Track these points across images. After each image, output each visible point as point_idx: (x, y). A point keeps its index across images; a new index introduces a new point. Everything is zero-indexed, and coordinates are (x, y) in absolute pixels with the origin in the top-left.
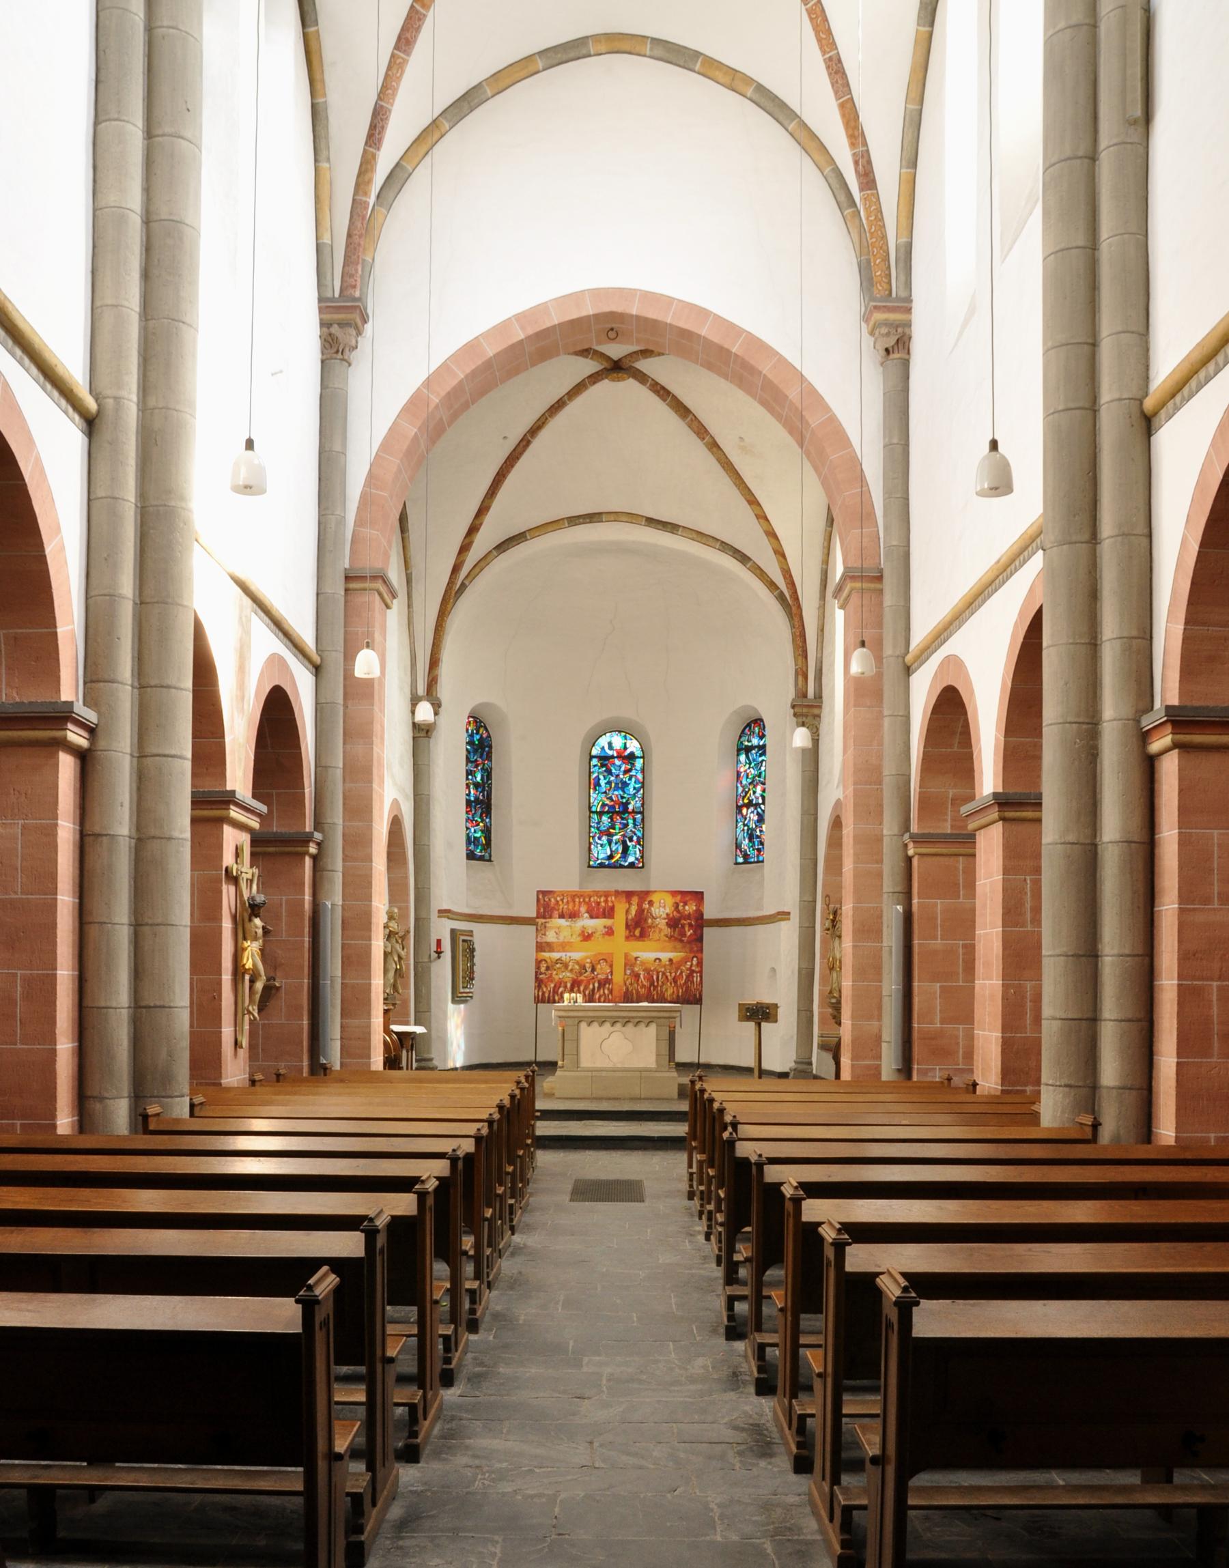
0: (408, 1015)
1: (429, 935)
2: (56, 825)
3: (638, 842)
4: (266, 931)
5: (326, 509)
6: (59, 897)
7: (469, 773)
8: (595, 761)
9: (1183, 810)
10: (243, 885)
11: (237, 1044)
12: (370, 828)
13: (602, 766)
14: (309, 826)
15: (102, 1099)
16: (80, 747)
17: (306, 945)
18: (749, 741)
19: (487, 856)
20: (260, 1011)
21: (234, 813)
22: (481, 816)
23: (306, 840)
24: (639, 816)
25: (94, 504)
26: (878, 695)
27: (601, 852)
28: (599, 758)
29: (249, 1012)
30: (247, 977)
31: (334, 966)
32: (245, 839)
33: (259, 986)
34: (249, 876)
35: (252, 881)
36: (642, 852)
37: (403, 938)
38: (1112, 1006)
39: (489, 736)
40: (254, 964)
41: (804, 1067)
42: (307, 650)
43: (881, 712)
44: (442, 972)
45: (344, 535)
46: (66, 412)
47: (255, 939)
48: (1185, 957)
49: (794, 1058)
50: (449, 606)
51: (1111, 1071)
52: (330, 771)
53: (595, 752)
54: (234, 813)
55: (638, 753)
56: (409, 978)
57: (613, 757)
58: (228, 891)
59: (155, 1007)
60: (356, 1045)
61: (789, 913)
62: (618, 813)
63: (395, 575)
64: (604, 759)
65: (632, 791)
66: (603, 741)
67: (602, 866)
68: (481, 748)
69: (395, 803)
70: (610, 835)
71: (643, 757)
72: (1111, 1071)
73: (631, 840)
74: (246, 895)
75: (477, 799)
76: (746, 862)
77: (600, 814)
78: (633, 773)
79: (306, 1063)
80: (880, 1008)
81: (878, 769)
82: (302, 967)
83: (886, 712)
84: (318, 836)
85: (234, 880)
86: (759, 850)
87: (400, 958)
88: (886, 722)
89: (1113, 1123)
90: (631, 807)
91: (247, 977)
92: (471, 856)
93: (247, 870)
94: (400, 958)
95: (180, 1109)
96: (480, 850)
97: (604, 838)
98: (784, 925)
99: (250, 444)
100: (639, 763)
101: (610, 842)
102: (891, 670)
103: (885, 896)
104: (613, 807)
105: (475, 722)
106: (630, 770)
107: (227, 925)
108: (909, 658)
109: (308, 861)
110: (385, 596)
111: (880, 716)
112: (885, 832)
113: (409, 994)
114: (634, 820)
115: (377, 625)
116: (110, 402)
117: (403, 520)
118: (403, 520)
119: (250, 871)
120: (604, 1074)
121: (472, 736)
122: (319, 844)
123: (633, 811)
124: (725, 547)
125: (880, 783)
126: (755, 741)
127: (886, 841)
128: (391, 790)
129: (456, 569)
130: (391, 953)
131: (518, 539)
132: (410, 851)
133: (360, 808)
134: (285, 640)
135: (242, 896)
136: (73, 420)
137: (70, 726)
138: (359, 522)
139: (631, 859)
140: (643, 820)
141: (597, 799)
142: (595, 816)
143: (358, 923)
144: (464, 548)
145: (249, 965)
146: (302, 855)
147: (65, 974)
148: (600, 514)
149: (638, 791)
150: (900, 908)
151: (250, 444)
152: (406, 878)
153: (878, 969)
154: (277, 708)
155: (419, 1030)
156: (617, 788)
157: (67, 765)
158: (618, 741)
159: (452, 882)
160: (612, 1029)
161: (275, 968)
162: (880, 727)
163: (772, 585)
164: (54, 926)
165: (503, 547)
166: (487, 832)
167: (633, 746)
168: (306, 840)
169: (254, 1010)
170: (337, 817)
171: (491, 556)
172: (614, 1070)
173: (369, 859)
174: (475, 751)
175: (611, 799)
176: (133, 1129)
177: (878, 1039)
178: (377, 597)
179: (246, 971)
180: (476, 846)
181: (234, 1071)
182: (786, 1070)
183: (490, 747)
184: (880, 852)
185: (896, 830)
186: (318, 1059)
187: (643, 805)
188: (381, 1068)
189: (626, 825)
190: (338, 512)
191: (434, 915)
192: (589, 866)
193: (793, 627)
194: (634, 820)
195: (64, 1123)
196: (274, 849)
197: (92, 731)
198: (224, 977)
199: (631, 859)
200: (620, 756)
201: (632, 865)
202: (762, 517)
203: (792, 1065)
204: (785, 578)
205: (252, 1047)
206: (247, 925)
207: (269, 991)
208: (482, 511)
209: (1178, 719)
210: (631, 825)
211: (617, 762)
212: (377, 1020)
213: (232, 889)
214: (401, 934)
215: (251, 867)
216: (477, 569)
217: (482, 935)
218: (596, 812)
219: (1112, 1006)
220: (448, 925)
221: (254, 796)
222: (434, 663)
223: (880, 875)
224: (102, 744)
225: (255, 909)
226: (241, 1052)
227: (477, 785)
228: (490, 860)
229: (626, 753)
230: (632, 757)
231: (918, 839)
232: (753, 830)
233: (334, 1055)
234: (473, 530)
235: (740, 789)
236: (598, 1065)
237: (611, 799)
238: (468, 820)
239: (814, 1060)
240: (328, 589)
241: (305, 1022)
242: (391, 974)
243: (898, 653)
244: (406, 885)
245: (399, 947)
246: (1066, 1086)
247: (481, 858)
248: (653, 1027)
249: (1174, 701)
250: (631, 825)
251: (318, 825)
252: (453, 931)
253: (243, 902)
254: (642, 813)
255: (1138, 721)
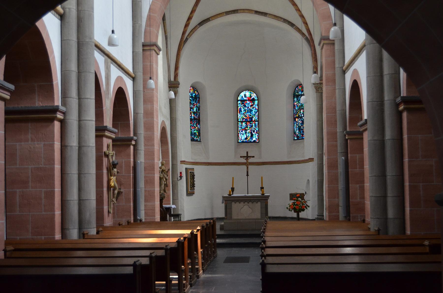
0: (169, 201)
1: (177, 171)
2: (54, 144)
3: (257, 133)
4: (118, 172)
5: (135, 22)
6: (55, 166)
7: (191, 108)
8: (239, 102)
9: (408, 129)
10: (110, 157)
11: (109, 212)
12: (153, 134)
13: (242, 104)
14: (132, 135)
15: (69, 229)
16: (60, 119)
17: (132, 177)
18: (298, 93)
19: (199, 140)
20: (116, 200)
21: (107, 133)
22: (196, 125)
23: (131, 139)
24: (257, 123)
25: (63, 42)
26: (334, 81)
27: (242, 137)
28: (241, 101)
29: (113, 201)
30: (112, 189)
31: (141, 184)
32: (110, 141)
33: (116, 192)
34: (112, 154)
35: (113, 156)
36: (258, 136)
37: (167, 172)
38: (390, 193)
39: (199, 94)
40: (114, 185)
41: (321, 217)
42: (130, 73)
43: (335, 87)
44: (182, 185)
45: (141, 30)
46: (54, 15)
47: (114, 176)
48: (411, 176)
49: (317, 214)
50: (182, 47)
51: (391, 213)
52: (139, 115)
53: (239, 98)
54: (107, 133)
55: (256, 98)
56: (170, 186)
57: (246, 100)
58: (105, 160)
59: (85, 200)
60: (150, 211)
61: (313, 159)
62: (249, 122)
63: (160, 42)
64: (243, 101)
65: (254, 113)
66: (242, 94)
67: (243, 142)
68: (196, 99)
69: (163, 122)
70: (246, 130)
71: (258, 100)
72: (391, 213)
73: (254, 132)
74: (111, 161)
75: (194, 118)
76: (298, 139)
77: (242, 122)
78: (254, 106)
79: (132, 219)
80: (338, 194)
81: (335, 108)
82: (130, 185)
83: (337, 88)
84: (135, 138)
85: (107, 156)
86: (303, 135)
87: (166, 180)
88: (337, 91)
89: (392, 230)
90: (253, 119)
91: (112, 189)
92: (193, 140)
93: (111, 152)
94: (166, 180)
95: (93, 232)
96: (196, 137)
97: (244, 131)
98: (311, 163)
99: (113, 32)
100: (256, 102)
101: (246, 133)
102: (338, 72)
103: (338, 154)
104: (247, 119)
105: (193, 89)
106: (253, 105)
107: (105, 171)
108: (344, 68)
109: (132, 147)
110: (157, 51)
111: (335, 89)
112: (338, 131)
113: (170, 193)
114: (255, 124)
115: (154, 62)
116: (67, 10)
117: (164, 19)
118: (164, 19)
119: (112, 153)
120: (242, 221)
121: (192, 94)
122: (136, 141)
123: (254, 121)
124: (285, 21)
125: (336, 113)
126: (300, 93)
127: (338, 134)
128: (161, 117)
129: (184, 33)
130: (163, 178)
131: (207, 20)
132: (168, 139)
133: (149, 127)
134: (122, 71)
135: (110, 161)
136: (56, 17)
137: (58, 113)
138: (147, 25)
139: (254, 139)
140: (258, 124)
141: (240, 116)
142: (240, 123)
143: (150, 168)
144: (187, 25)
145: (113, 185)
146: (129, 146)
147: (57, 190)
148: (238, 10)
149: (256, 113)
150: (343, 158)
151: (113, 32)
152: (168, 149)
153: (337, 180)
154: (120, 94)
155: (173, 206)
156: (248, 112)
157: (57, 124)
158: (248, 94)
159: (185, 150)
160: (244, 204)
161: (121, 185)
162: (335, 92)
163: (303, 34)
164: (53, 176)
165: (201, 24)
166: (199, 130)
167: (254, 96)
168: (131, 139)
169: (114, 200)
170: (141, 131)
171: (197, 27)
172: (246, 219)
173: (153, 145)
174: (193, 100)
175: (246, 116)
176: (79, 237)
177: (338, 205)
178: (154, 52)
179: (112, 187)
180: (195, 136)
181: (108, 222)
182: (314, 218)
183: (199, 98)
184: (336, 138)
185: (341, 130)
186: (137, 217)
187: (258, 118)
188: (159, 220)
189: (252, 126)
190: (139, 23)
191: (179, 163)
192: (238, 142)
193: (311, 50)
194: (255, 124)
195: (58, 236)
196: (122, 144)
197: (64, 113)
198: (104, 189)
199: (254, 139)
200: (248, 100)
201: (254, 141)
202: (298, 10)
203: (316, 217)
204: (308, 32)
205: (114, 213)
206: (112, 171)
207: (119, 193)
208: (193, 11)
209: (405, 101)
210: (254, 126)
211: (248, 102)
212: (157, 203)
213: (106, 159)
214: (166, 171)
215: (113, 151)
216: (192, 33)
217: (198, 170)
218: (240, 121)
219: (390, 193)
220: (185, 166)
221: (114, 126)
222: (177, 68)
223: (336, 146)
224: (67, 117)
225: (114, 165)
226: (110, 214)
227: (194, 113)
228: (200, 141)
229: (251, 99)
230: (253, 100)
231: (349, 133)
232: (300, 127)
233: (142, 215)
234: (190, 18)
235: (295, 111)
236: (239, 218)
237: (246, 116)
238: (191, 126)
239: (324, 214)
240: (136, 50)
241: (132, 204)
242: (163, 186)
243: (340, 66)
244: (168, 152)
245: (166, 176)
246: (377, 218)
247: (197, 141)
248: (259, 204)
249: (405, 95)
250: (254, 126)
251: (135, 134)
252: (186, 169)
253: (110, 164)
254: (258, 121)
255: (395, 101)
